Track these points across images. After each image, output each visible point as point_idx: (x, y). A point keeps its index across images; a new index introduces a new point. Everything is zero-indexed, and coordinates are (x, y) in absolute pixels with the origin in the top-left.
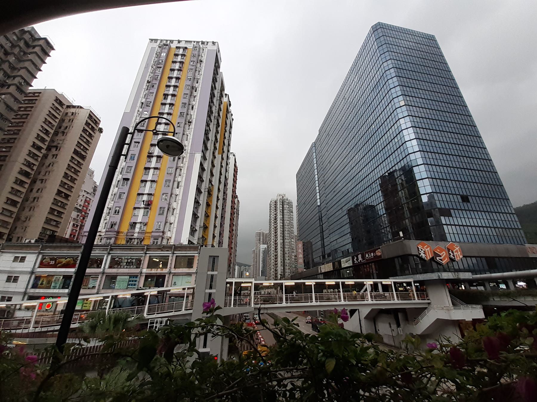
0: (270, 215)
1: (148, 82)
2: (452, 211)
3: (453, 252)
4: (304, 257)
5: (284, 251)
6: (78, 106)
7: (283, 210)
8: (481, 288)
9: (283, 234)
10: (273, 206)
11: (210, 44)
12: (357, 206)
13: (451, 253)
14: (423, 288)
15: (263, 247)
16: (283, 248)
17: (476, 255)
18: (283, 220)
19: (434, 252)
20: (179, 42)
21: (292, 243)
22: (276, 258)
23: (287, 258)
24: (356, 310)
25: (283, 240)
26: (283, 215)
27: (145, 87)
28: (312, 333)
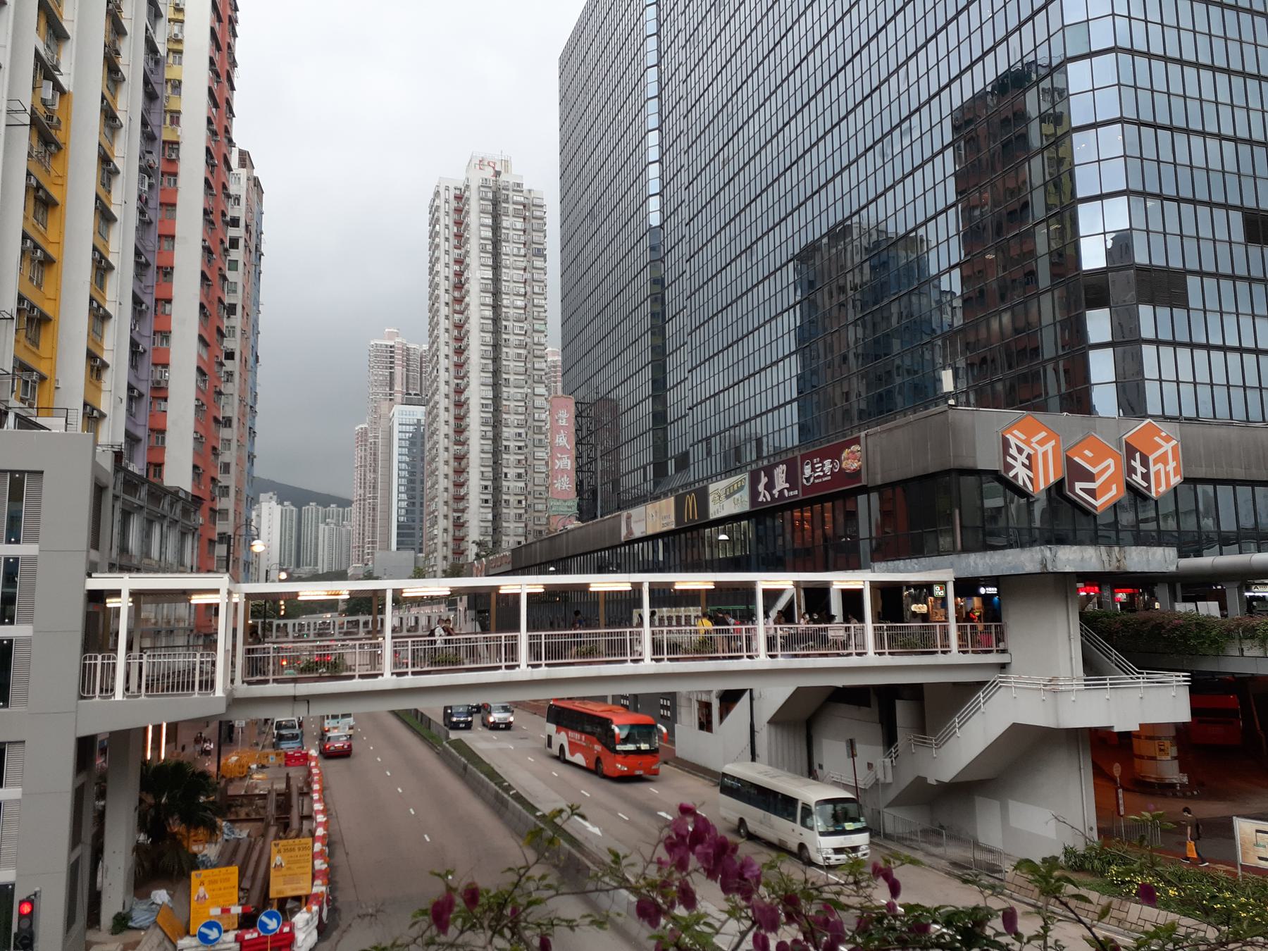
0: (434, 261)
2: (1193, 282)
3: (1145, 462)
4: (579, 469)
5: (496, 438)
7: (496, 242)
8: (1210, 609)
9: (496, 359)
10: (446, 220)
12: (839, 233)
13: (1137, 464)
14: (988, 609)
15: (405, 416)
16: (496, 423)
17: (1239, 474)
18: (496, 294)
19: (1070, 461)
21: (539, 402)
22: (459, 471)
23: (512, 472)
24: (740, 693)
25: (496, 386)
26: (496, 267)
28: (219, 821)
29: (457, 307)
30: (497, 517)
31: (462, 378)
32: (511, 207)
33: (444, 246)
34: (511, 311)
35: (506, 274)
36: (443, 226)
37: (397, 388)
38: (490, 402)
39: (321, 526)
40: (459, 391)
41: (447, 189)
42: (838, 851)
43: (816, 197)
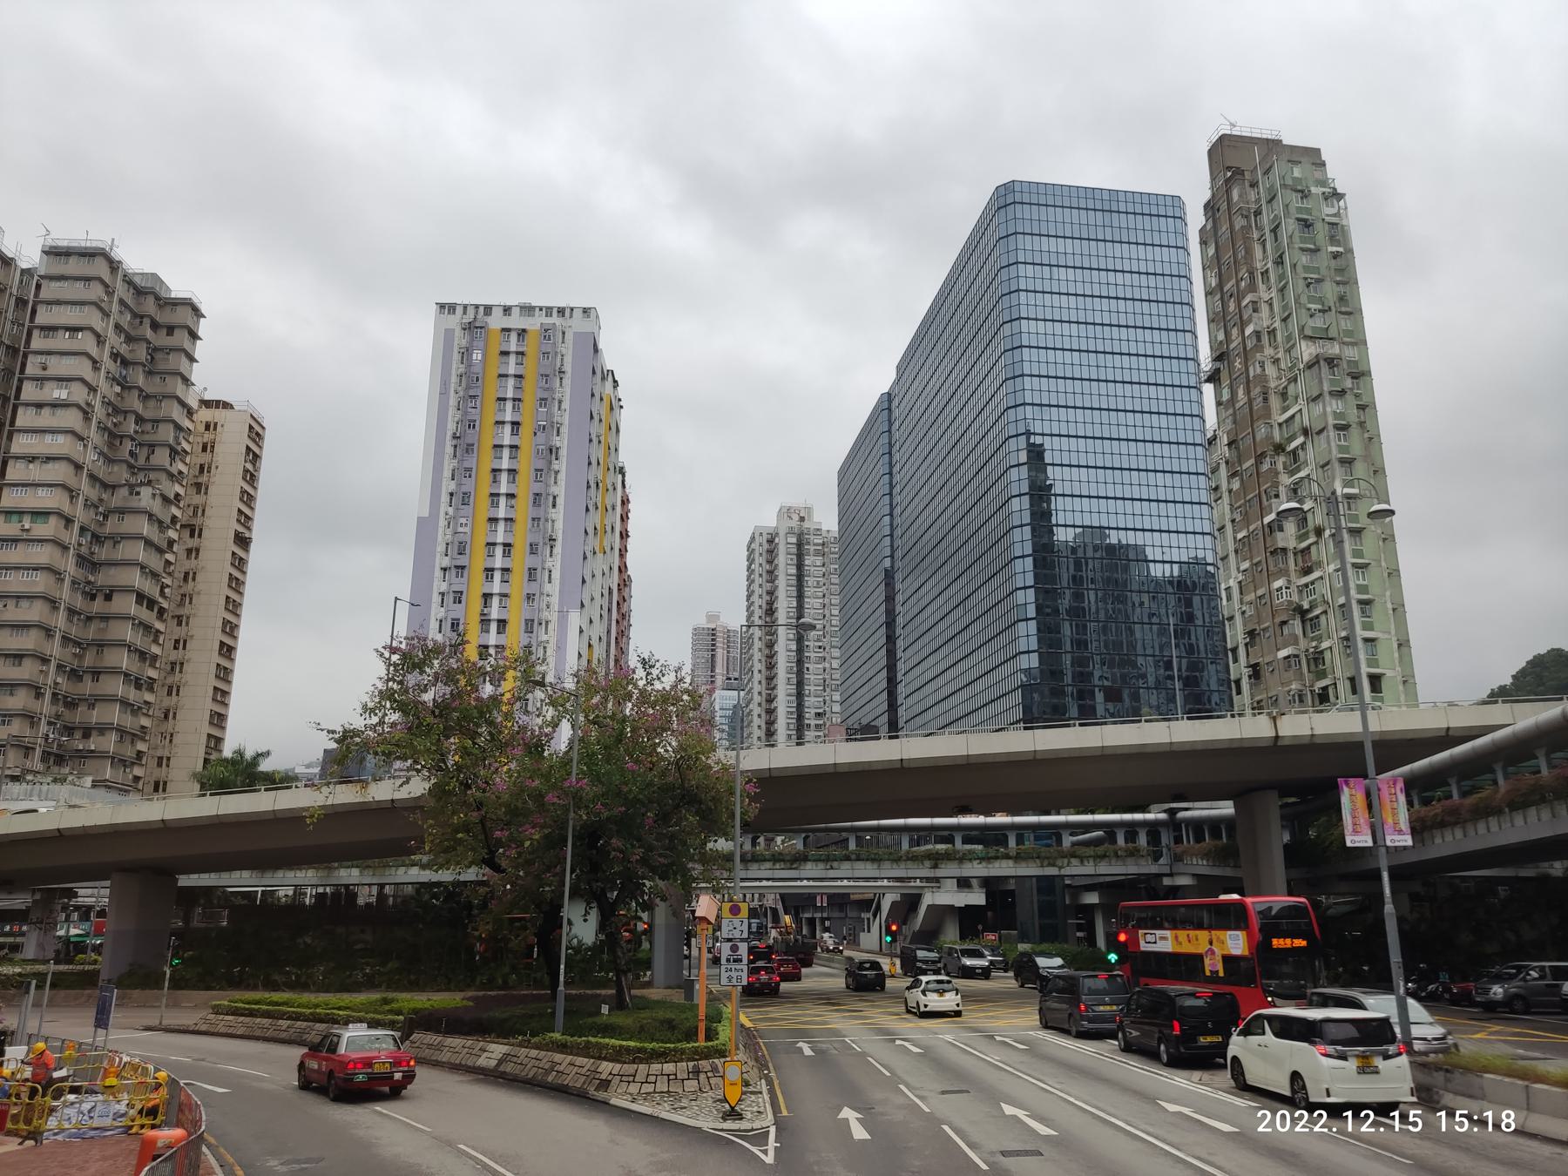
1: (455, 437)
6: (218, 402)
11: (578, 314)
20: (507, 310)
27: (449, 450)
32: (812, 548)
33: (758, 581)
37: (718, 670)
42: (1228, 589)
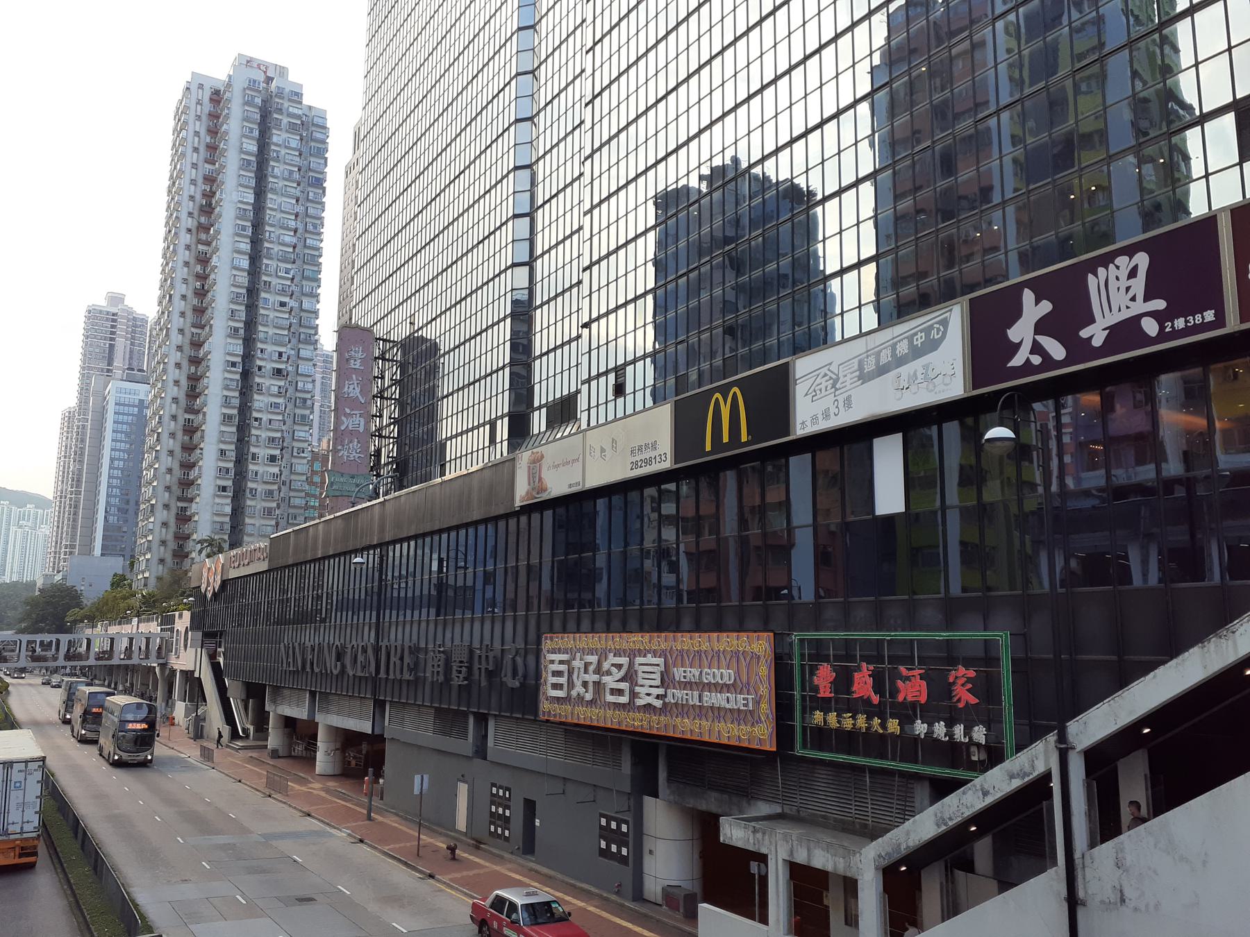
9: (252, 308)
16: (243, 421)
23: (263, 452)
29: (203, 236)
30: (237, 513)
31: (203, 327)
32: (285, 120)
34: (276, 248)
35: (272, 200)
36: (191, 133)
38: (239, 360)
39: (13, 529)
40: (197, 344)
41: (201, 86)
43: (632, 187)
